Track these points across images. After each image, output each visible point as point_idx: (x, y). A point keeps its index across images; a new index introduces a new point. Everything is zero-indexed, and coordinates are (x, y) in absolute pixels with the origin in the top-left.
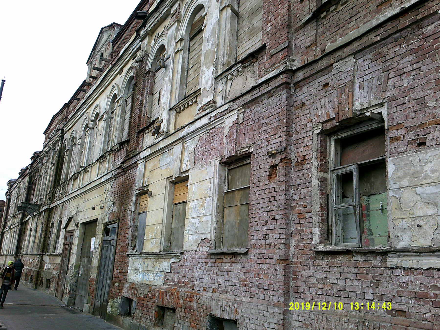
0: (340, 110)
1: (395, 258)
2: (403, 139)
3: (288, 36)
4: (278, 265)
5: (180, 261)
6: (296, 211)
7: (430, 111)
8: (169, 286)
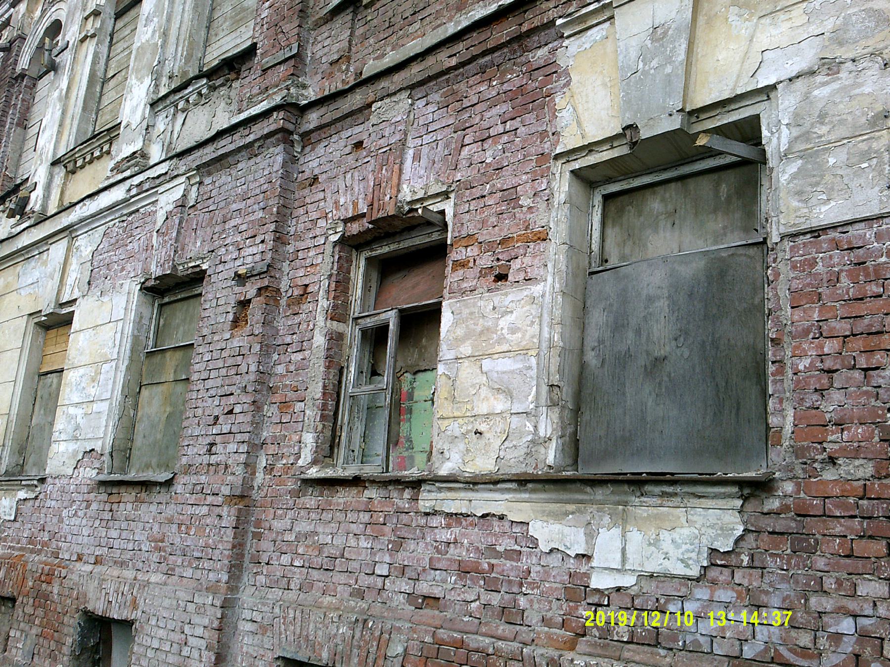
0: (375, 198)
1: (433, 494)
2: (472, 266)
3: (298, 34)
4: (225, 508)
5: (36, 498)
6: (277, 398)
7: (522, 216)
8: (9, 551)
